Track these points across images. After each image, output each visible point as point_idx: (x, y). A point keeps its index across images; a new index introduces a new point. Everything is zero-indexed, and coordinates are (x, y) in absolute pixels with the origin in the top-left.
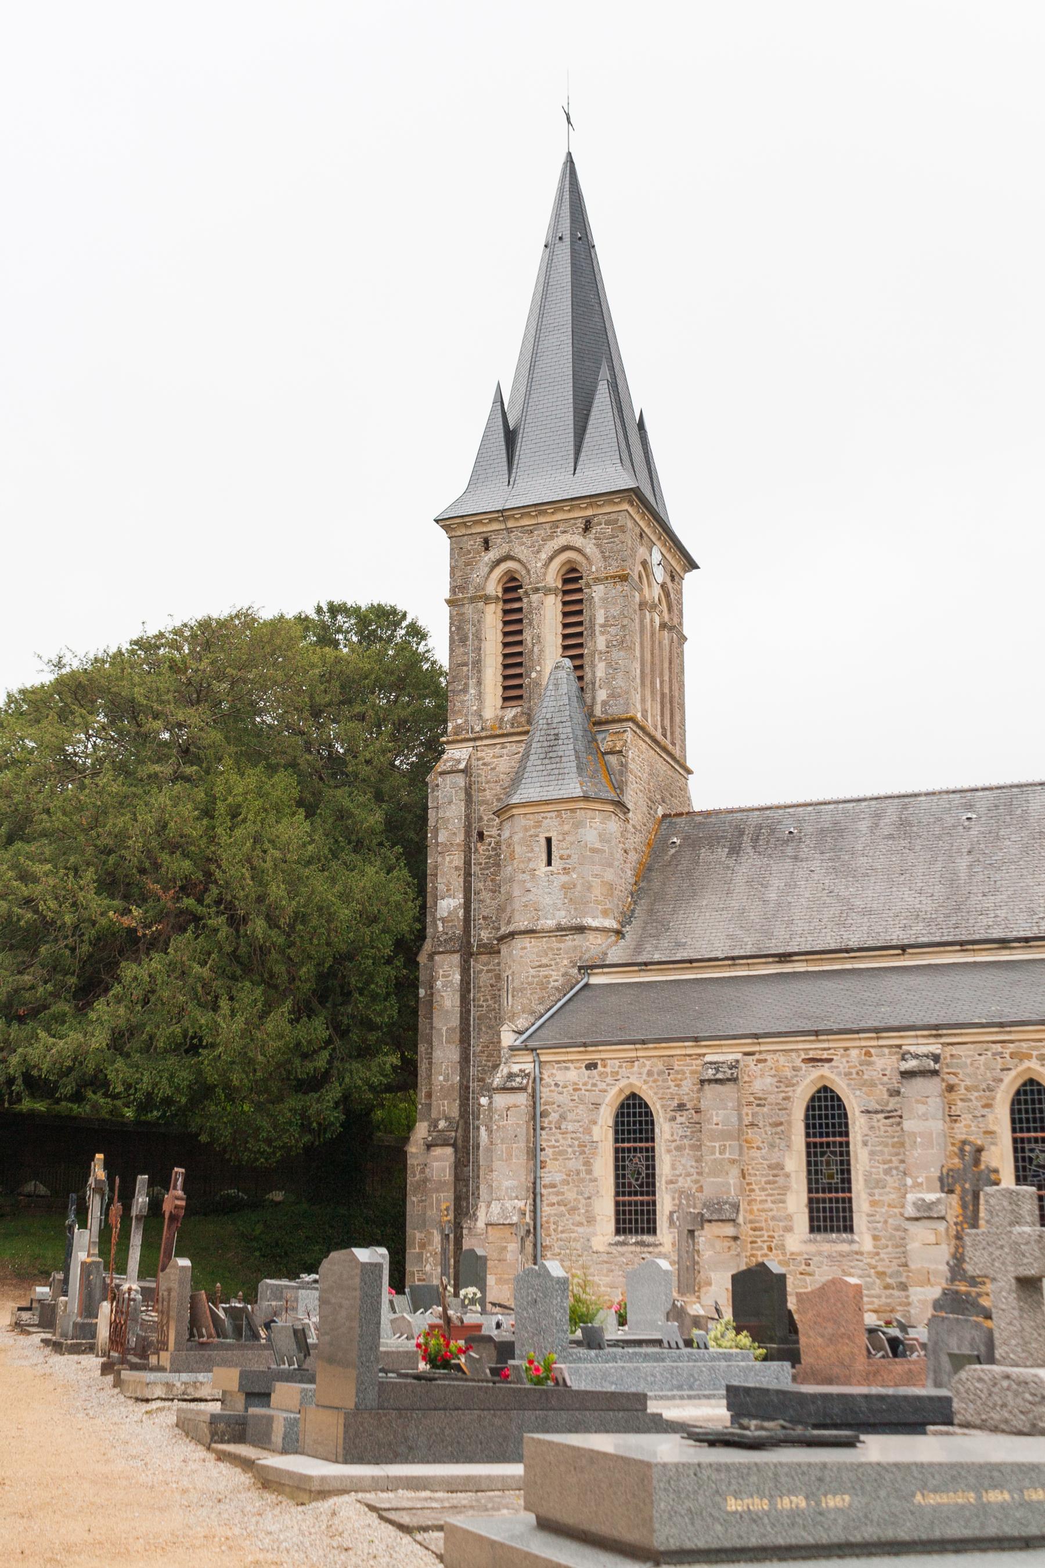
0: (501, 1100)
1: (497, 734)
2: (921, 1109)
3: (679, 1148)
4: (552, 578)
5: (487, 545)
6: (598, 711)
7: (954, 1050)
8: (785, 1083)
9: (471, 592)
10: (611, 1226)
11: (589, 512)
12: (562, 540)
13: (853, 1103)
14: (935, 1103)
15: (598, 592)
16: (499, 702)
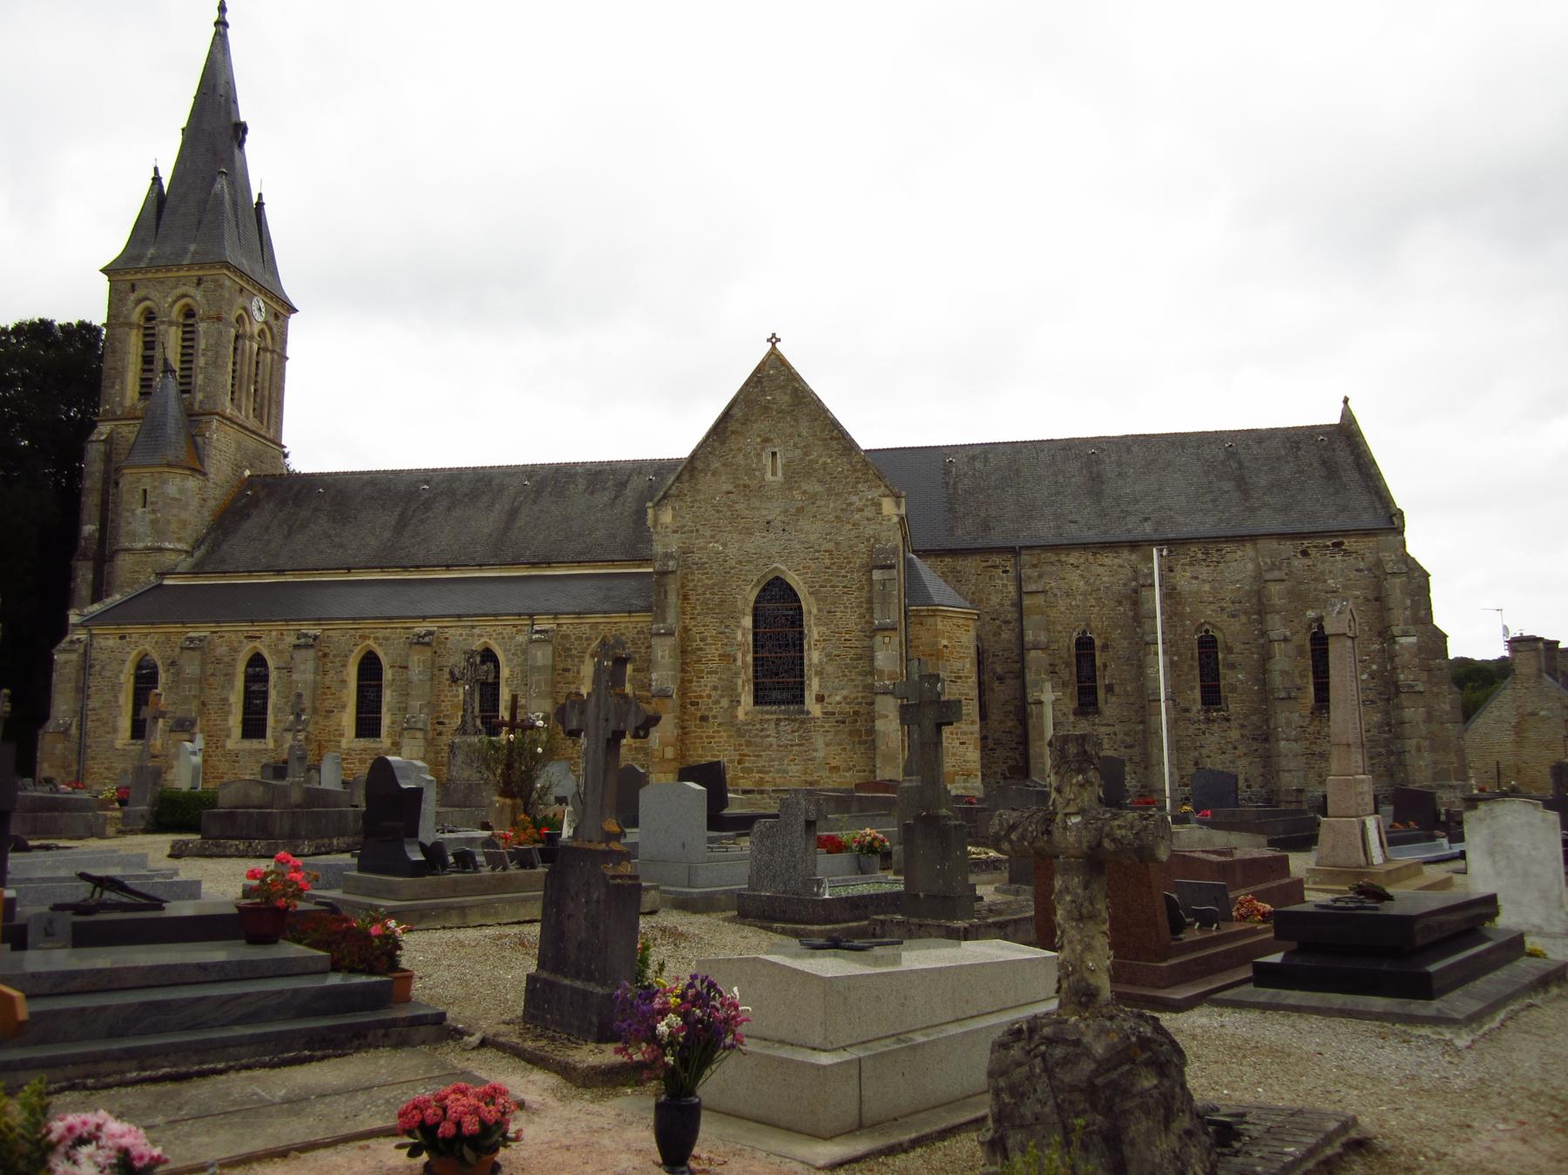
1: (130, 417)
2: (303, 667)
5: (133, 288)
7: (330, 633)
10: (128, 734)
12: (179, 292)
14: (310, 665)
15: (202, 327)
16: (137, 396)
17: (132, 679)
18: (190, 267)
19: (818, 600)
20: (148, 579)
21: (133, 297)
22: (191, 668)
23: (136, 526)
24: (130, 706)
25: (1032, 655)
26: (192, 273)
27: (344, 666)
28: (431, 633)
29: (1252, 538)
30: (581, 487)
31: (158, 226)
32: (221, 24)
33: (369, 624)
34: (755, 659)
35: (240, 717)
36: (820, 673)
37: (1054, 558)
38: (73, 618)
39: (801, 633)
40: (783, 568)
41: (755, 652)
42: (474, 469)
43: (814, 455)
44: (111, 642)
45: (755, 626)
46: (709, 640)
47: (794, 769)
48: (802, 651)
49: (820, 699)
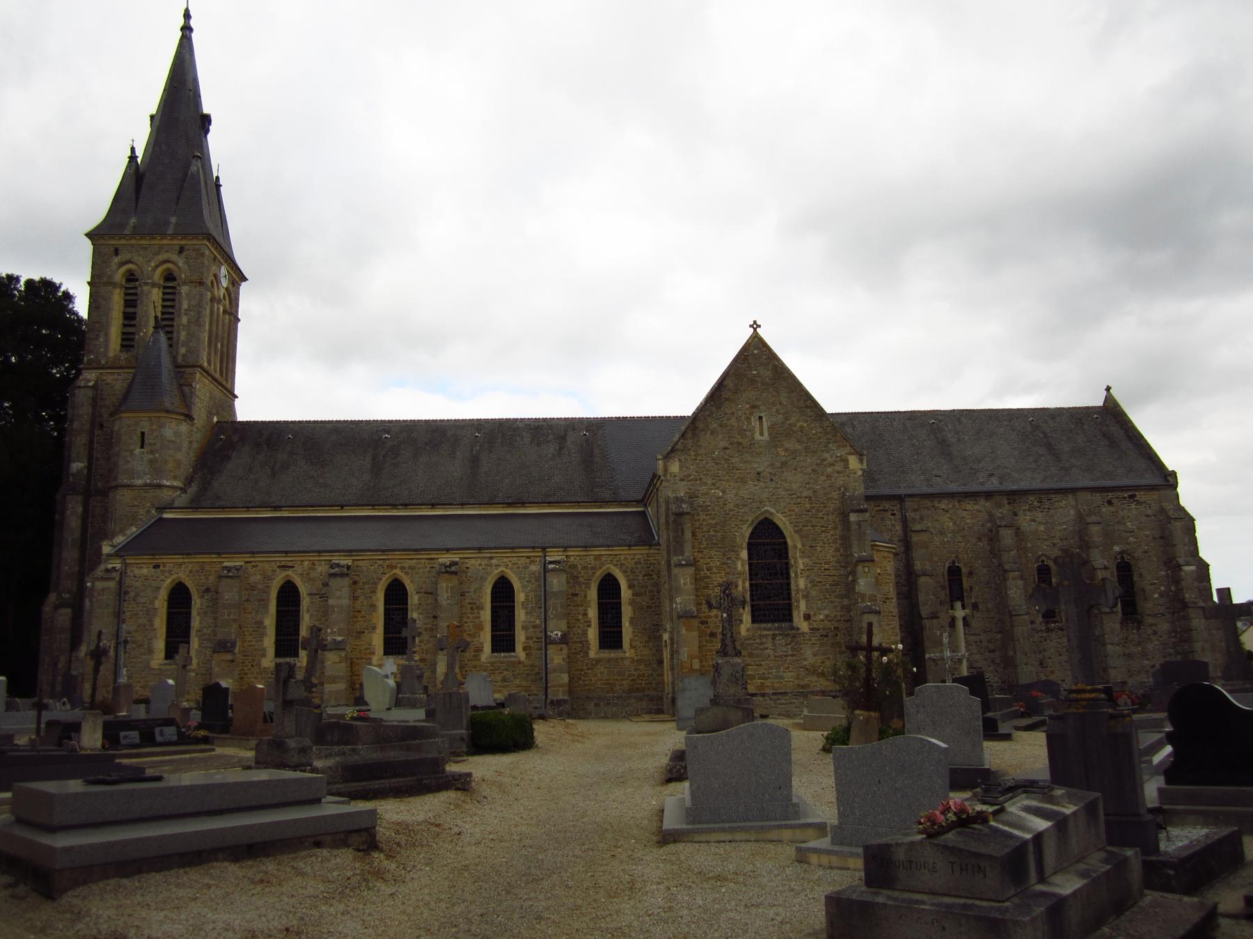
0: (99, 585)
1: (114, 366)
2: (338, 593)
3: (205, 613)
4: (158, 276)
6: (180, 359)
7: (359, 563)
8: (268, 578)
9: (105, 279)
10: (163, 655)
11: (183, 242)
12: (161, 257)
13: (303, 589)
14: (346, 591)
15: (184, 290)
16: (118, 348)
17: (165, 604)
18: (173, 236)
19: (802, 537)
20: (147, 515)
21: (116, 260)
22: (230, 594)
23: (135, 465)
24: (164, 630)
25: (923, 580)
26: (175, 242)
27: (374, 592)
28: (455, 564)
29: (1074, 490)
30: (527, 440)
31: (137, 199)
32: (187, 29)
33: (397, 555)
34: (751, 585)
35: (273, 639)
36: (806, 597)
37: (929, 504)
38: (106, 549)
39: (787, 564)
40: (772, 510)
41: (751, 579)
42: (566, 419)
43: (793, 420)
44: (145, 571)
45: (750, 558)
46: (714, 570)
47: (789, 675)
48: (788, 578)
49: (807, 617)
